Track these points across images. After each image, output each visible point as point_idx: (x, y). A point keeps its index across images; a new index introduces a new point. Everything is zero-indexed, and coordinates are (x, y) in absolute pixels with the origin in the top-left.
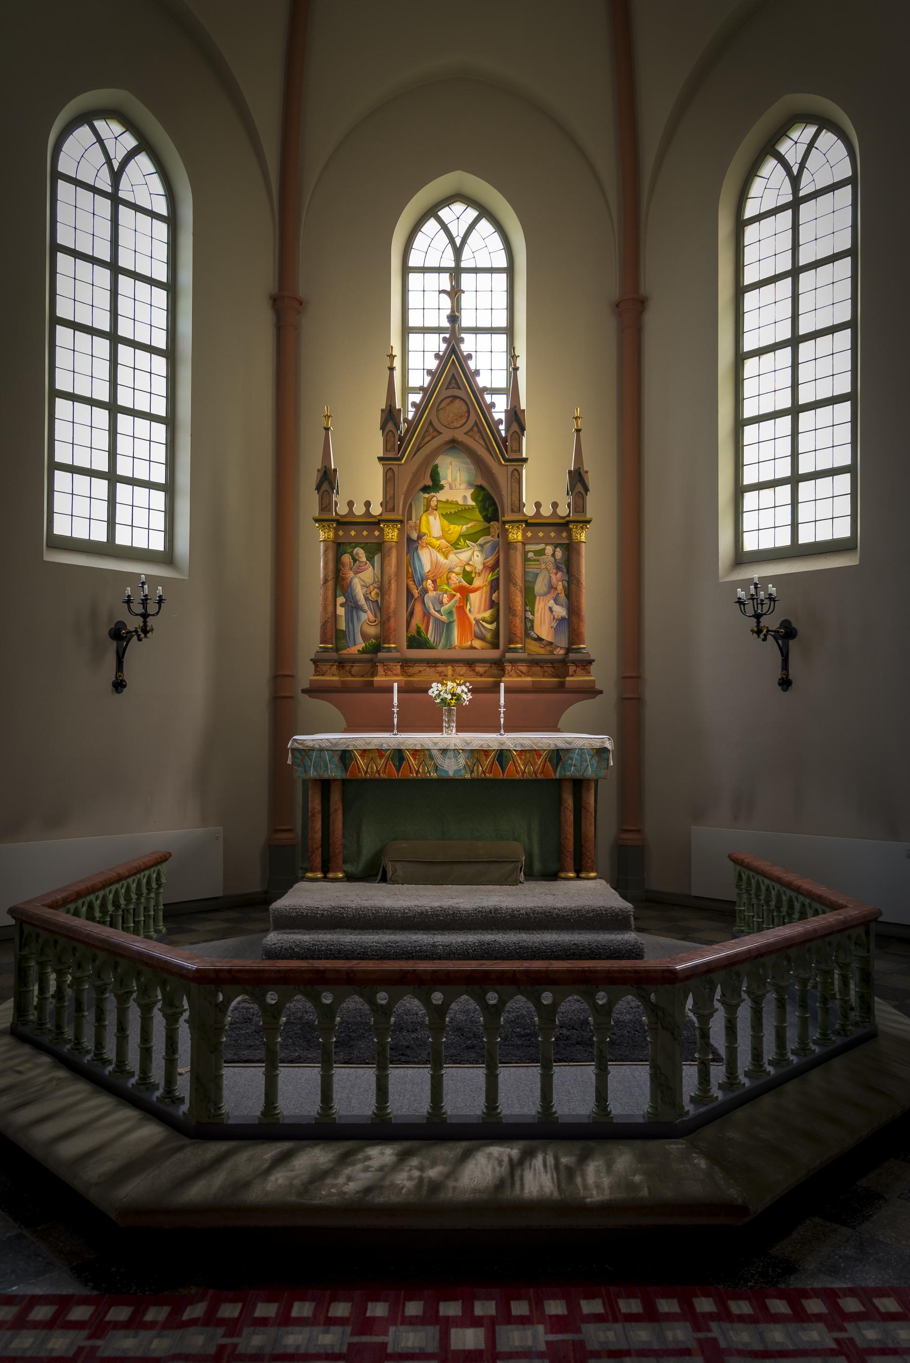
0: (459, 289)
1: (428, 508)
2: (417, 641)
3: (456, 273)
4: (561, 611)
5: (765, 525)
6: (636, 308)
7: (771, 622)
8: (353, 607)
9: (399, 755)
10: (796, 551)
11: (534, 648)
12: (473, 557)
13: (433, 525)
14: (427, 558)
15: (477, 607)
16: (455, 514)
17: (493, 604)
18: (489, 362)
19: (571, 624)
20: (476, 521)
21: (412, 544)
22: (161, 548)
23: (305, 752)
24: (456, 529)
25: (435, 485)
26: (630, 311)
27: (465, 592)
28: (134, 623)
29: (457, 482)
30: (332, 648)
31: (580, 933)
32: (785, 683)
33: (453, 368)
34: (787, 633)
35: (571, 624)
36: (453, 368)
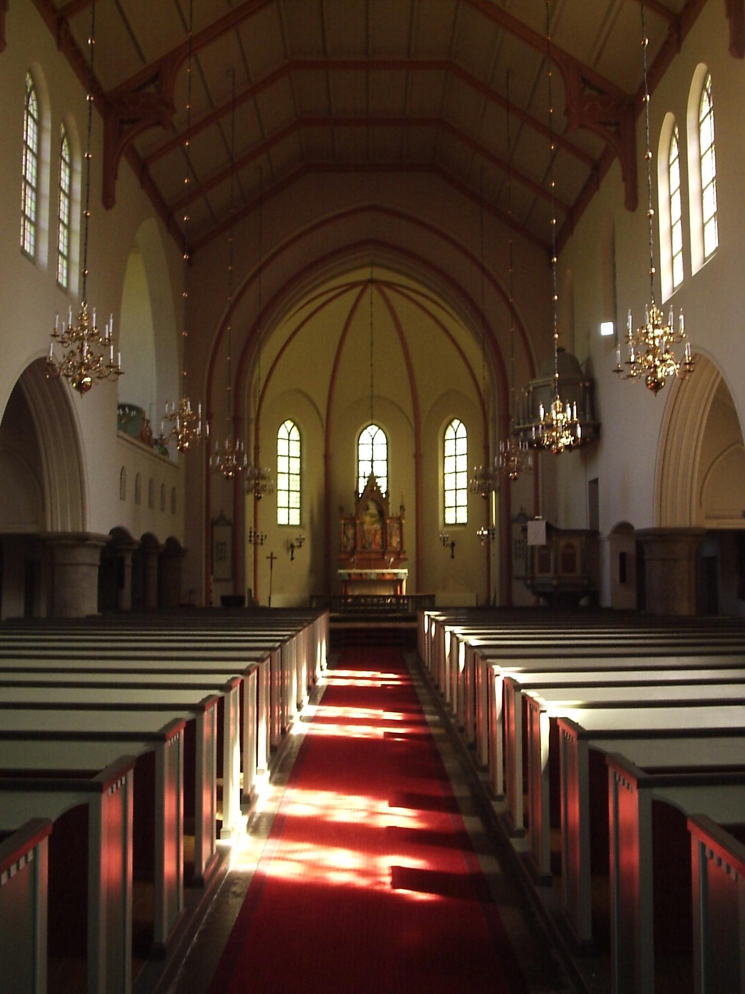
0: (373, 453)
1: (366, 514)
2: (364, 547)
3: (372, 461)
4: (399, 540)
5: (450, 518)
6: (418, 459)
7: (449, 542)
8: (348, 539)
9: (361, 574)
10: (456, 524)
11: (392, 549)
12: (377, 526)
13: (367, 519)
14: (366, 527)
15: (378, 538)
16: (372, 516)
17: (382, 538)
18: (382, 483)
19: (401, 543)
20: (377, 518)
21: (362, 523)
22: (297, 522)
23: (340, 574)
24: (373, 519)
25: (367, 509)
26: (418, 457)
27: (375, 535)
28: (296, 544)
29: (373, 509)
30: (224, 447)
31: (317, 878)
32: (453, 557)
33: (372, 479)
34: (453, 545)
35: (401, 543)
36: (372, 479)
